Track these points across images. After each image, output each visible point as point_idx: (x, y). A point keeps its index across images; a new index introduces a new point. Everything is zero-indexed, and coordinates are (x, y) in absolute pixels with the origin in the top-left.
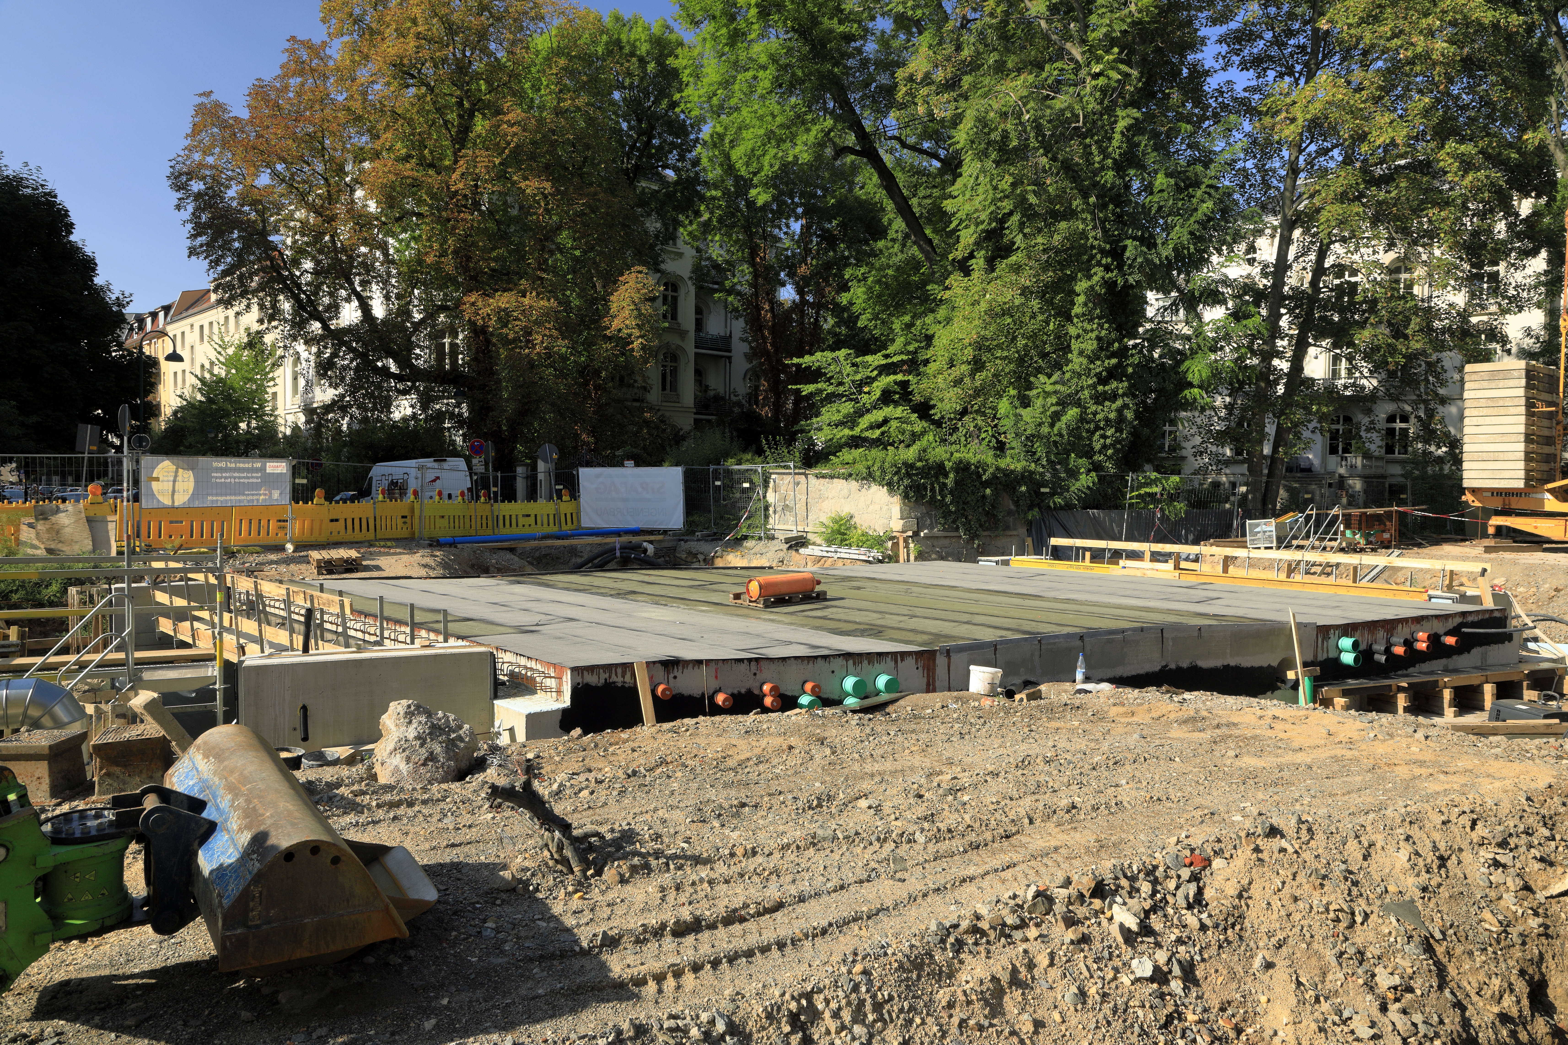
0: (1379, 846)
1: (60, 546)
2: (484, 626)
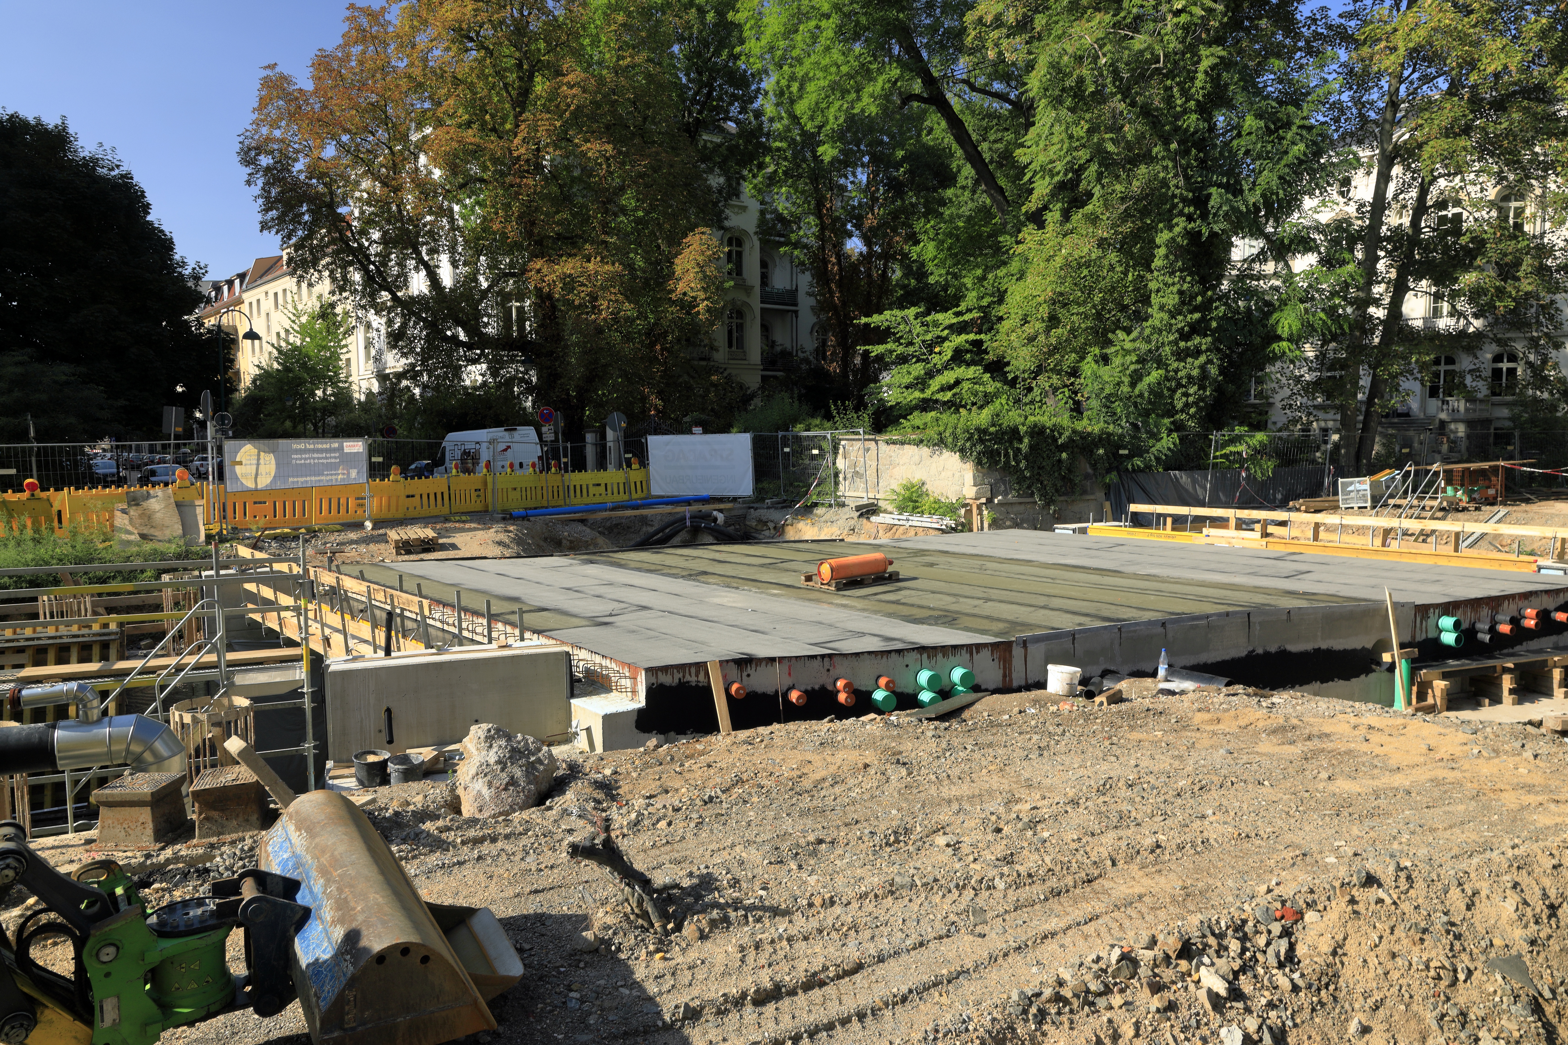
0: (1483, 894)
1: (152, 531)
2: (558, 617)
